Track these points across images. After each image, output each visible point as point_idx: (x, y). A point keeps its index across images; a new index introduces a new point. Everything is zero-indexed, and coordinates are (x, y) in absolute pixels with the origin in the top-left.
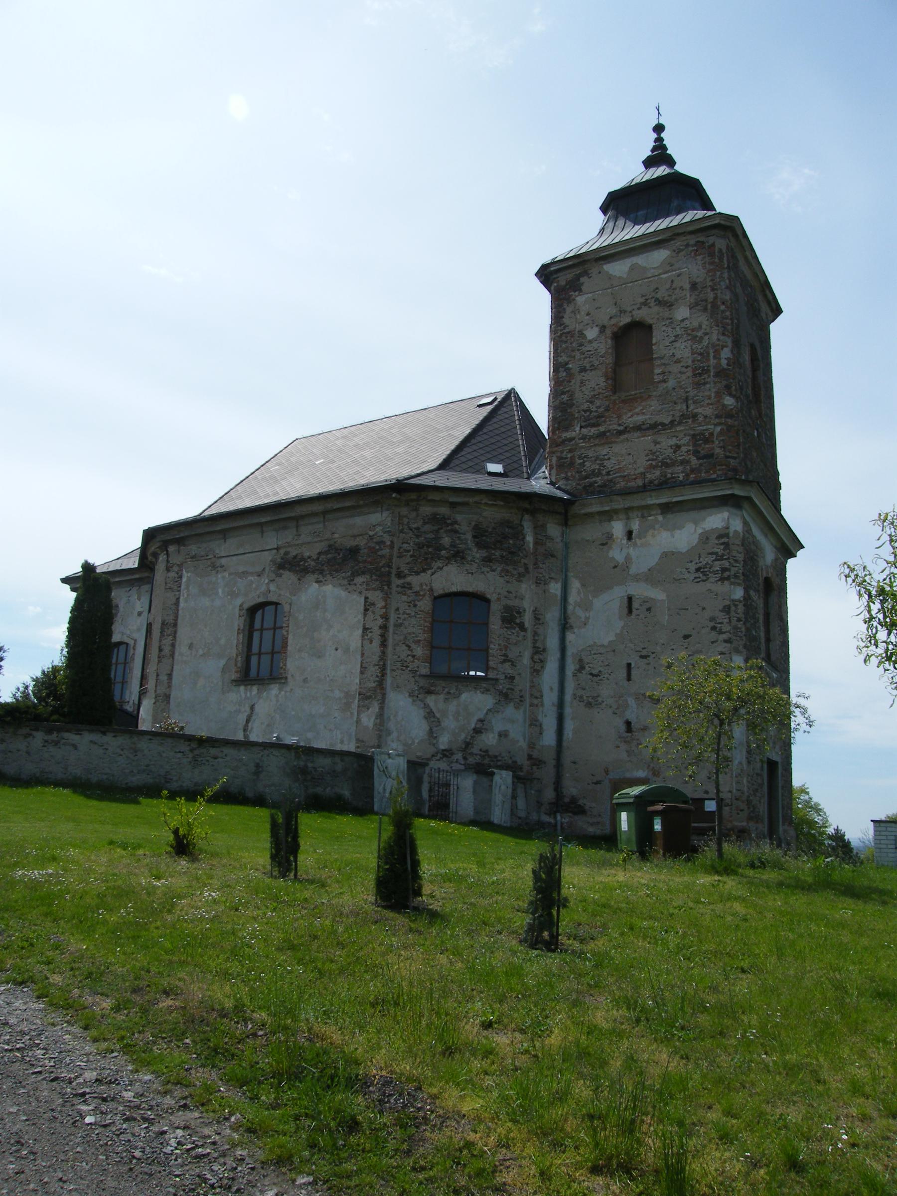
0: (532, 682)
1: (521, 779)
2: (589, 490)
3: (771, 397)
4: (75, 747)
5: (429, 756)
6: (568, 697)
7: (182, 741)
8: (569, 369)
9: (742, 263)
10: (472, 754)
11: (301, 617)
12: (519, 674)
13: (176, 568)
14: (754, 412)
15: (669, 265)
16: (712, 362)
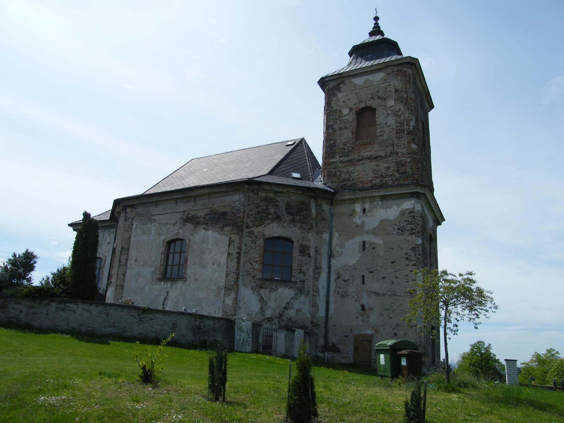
0: (314, 283)
1: (308, 334)
2: (344, 188)
3: (430, 147)
4: (74, 312)
5: (260, 321)
6: (332, 292)
7: (134, 310)
8: (334, 128)
9: (418, 81)
10: (283, 320)
11: (195, 247)
12: (307, 280)
13: (130, 220)
14: (424, 153)
15: (384, 80)
16: (406, 127)
